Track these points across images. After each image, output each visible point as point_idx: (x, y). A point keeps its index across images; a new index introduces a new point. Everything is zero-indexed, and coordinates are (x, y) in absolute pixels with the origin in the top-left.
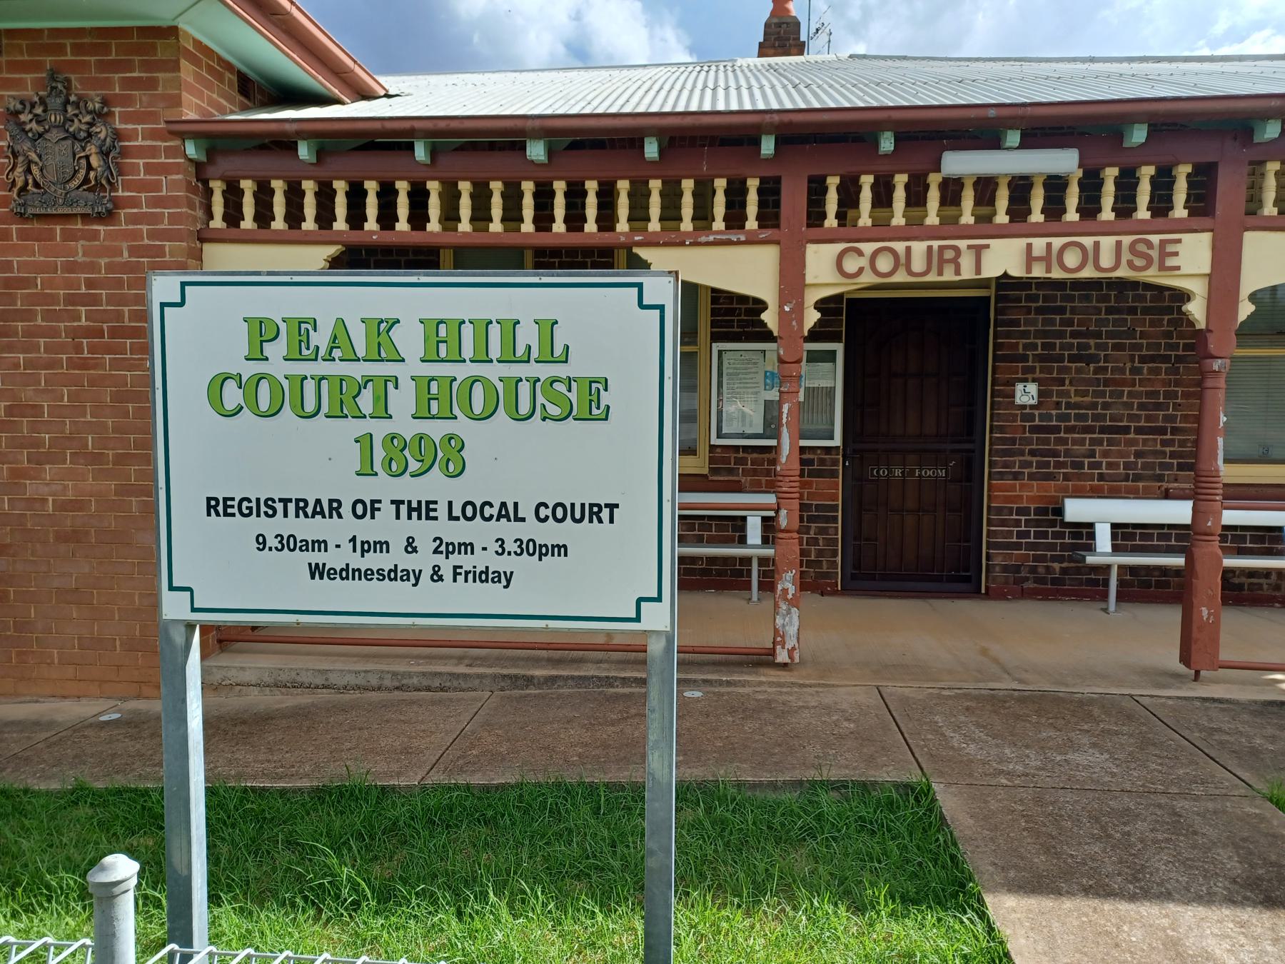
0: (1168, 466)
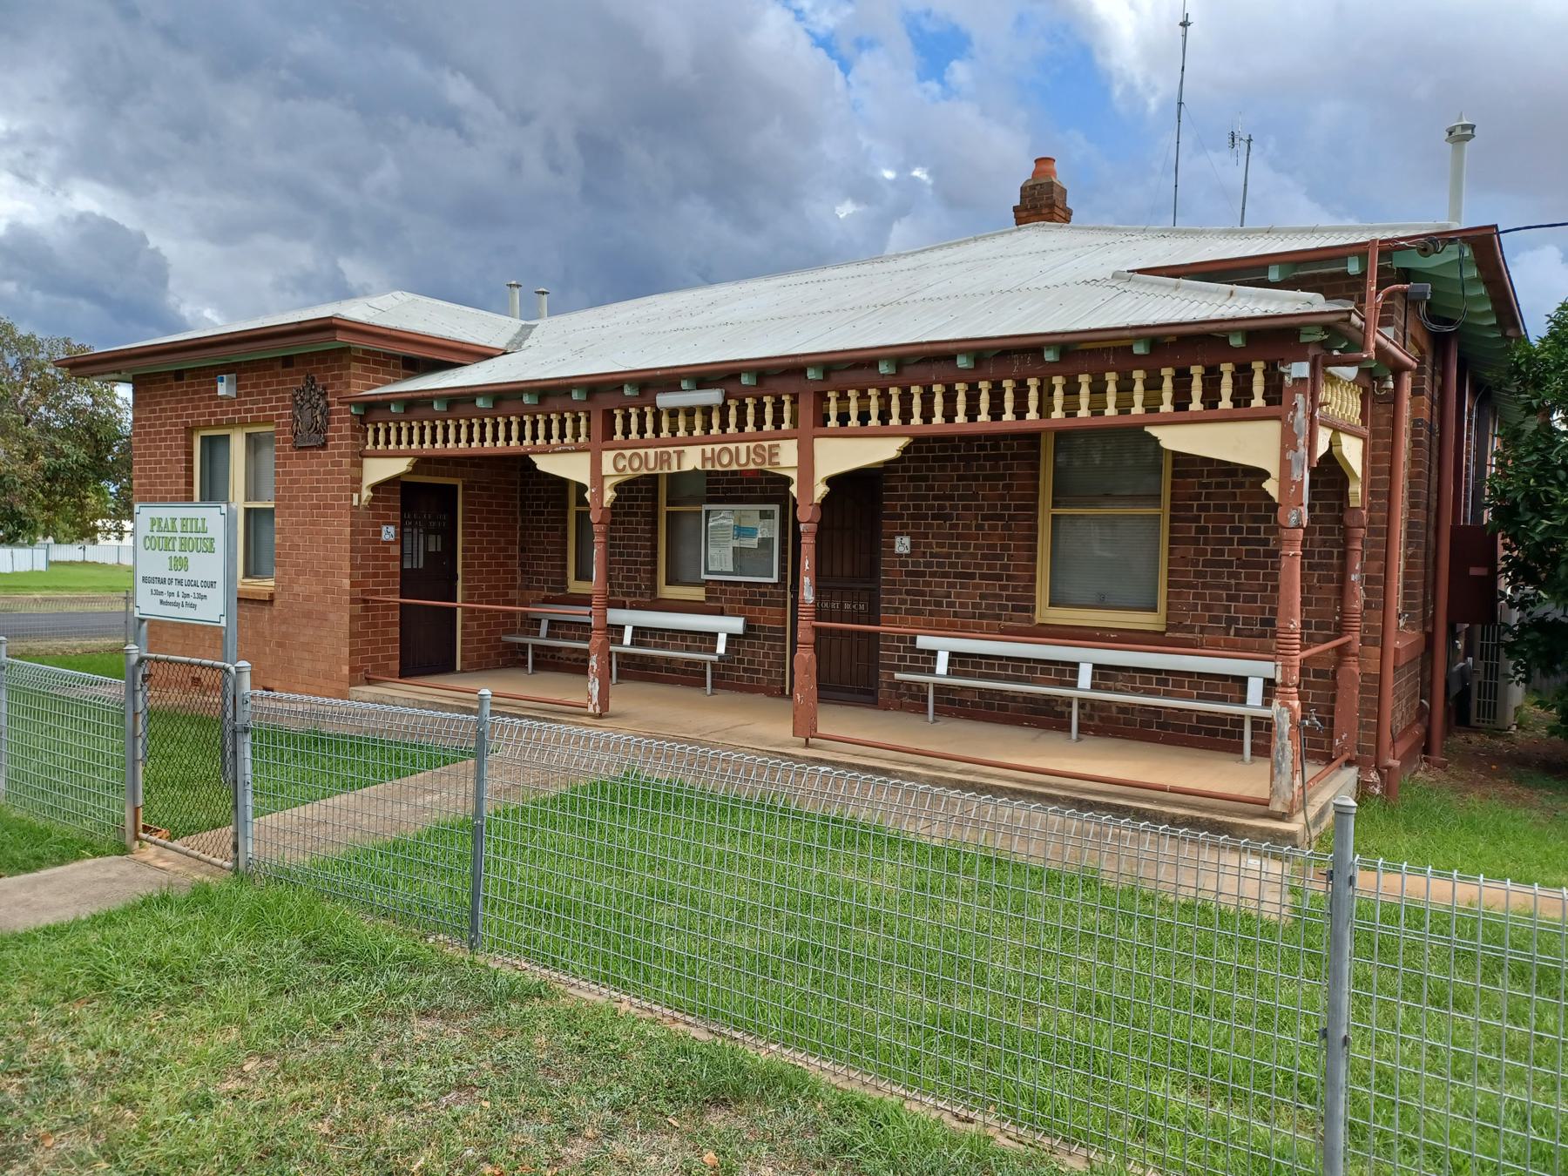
0: (1004, 608)
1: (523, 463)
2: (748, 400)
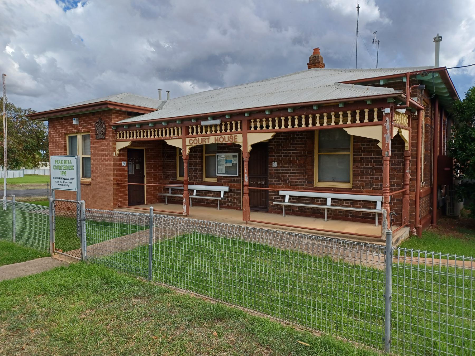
0: (305, 182)
1: (163, 142)
2: (228, 123)
